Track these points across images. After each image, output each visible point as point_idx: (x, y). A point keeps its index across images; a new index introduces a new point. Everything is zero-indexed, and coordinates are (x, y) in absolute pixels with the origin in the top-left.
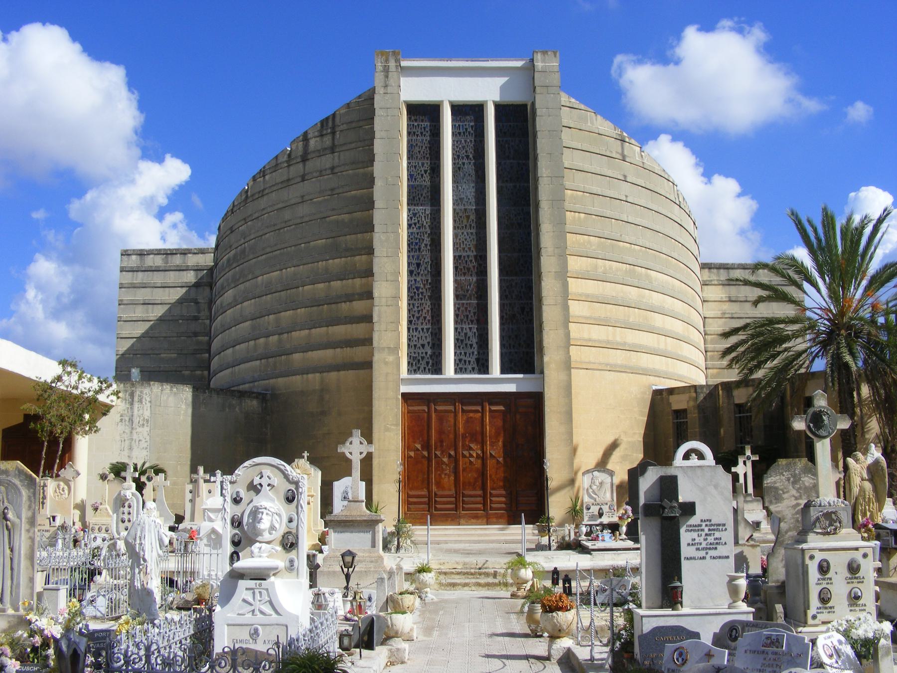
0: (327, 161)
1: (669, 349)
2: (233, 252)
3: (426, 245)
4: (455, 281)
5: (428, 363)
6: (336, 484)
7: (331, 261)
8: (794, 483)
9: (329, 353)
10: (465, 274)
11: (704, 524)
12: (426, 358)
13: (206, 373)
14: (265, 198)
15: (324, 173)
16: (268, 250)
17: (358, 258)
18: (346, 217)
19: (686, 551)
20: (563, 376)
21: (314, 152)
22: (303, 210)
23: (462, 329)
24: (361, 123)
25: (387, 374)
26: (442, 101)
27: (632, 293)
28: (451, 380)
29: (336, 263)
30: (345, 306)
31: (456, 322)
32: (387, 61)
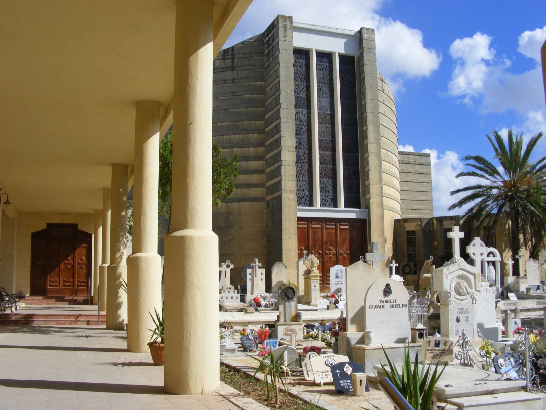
3: (304, 132)
4: (320, 154)
5: (306, 200)
7: (232, 136)
10: (324, 150)
12: (306, 199)
15: (227, 82)
17: (251, 135)
18: (243, 110)
20: (380, 211)
21: (219, 68)
23: (323, 181)
25: (290, 205)
26: (312, 49)
28: (318, 211)
29: (237, 137)
30: (243, 164)
31: (320, 177)
32: (285, 21)
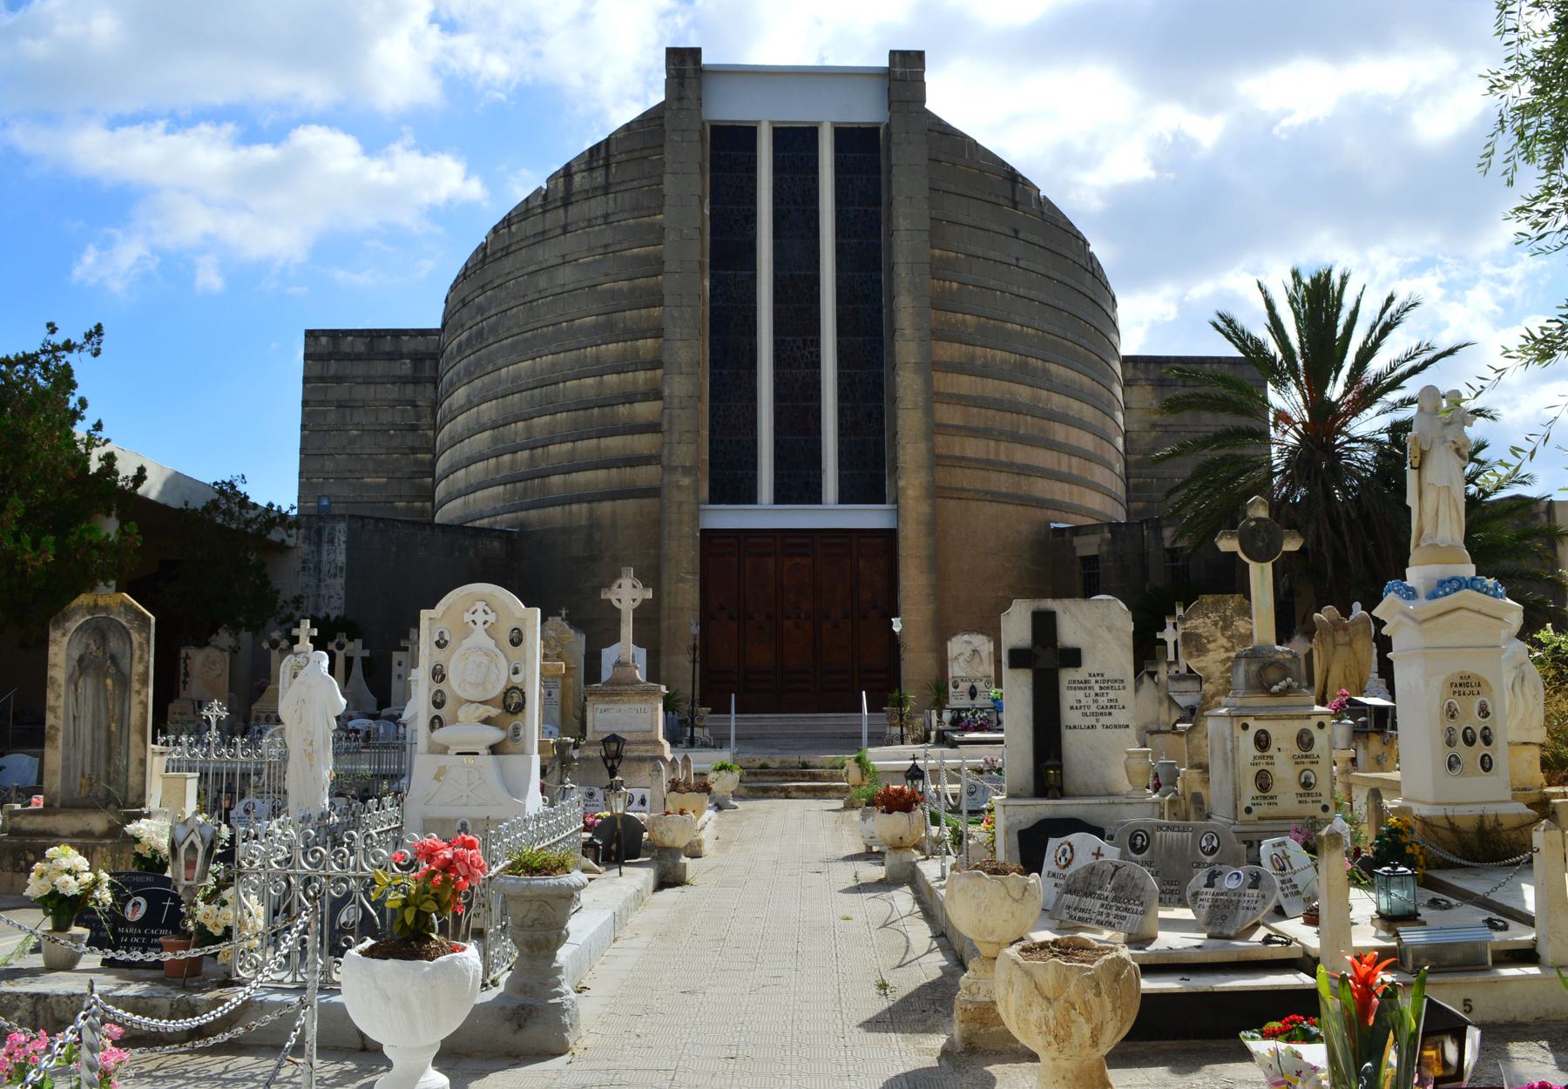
0: (597, 207)
1: (1075, 472)
2: (465, 335)
6: (605, 652)
7: (603, 347)
8: (1224, 629)
9: (601, 474)
11: (1093, 680)
13: (428, 504)
14: (511, 257)
16: (515, 331)
17: (640, 342)
18: (625, 285)
19: (1069, 716)
22: (566, 276)
24: (646, 152)
27: (1023, 393)
28: (765, 514)
30: (623, 410)
